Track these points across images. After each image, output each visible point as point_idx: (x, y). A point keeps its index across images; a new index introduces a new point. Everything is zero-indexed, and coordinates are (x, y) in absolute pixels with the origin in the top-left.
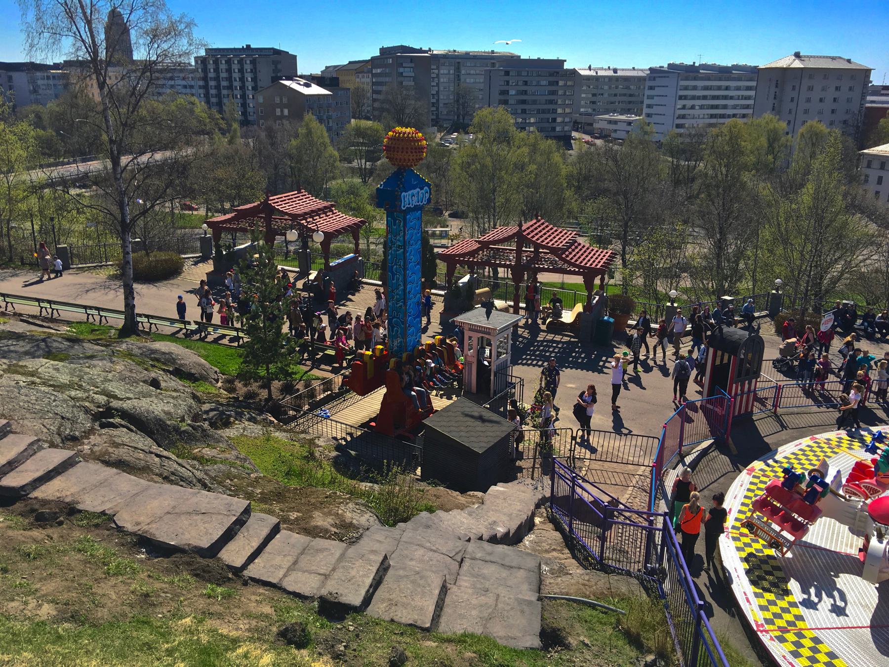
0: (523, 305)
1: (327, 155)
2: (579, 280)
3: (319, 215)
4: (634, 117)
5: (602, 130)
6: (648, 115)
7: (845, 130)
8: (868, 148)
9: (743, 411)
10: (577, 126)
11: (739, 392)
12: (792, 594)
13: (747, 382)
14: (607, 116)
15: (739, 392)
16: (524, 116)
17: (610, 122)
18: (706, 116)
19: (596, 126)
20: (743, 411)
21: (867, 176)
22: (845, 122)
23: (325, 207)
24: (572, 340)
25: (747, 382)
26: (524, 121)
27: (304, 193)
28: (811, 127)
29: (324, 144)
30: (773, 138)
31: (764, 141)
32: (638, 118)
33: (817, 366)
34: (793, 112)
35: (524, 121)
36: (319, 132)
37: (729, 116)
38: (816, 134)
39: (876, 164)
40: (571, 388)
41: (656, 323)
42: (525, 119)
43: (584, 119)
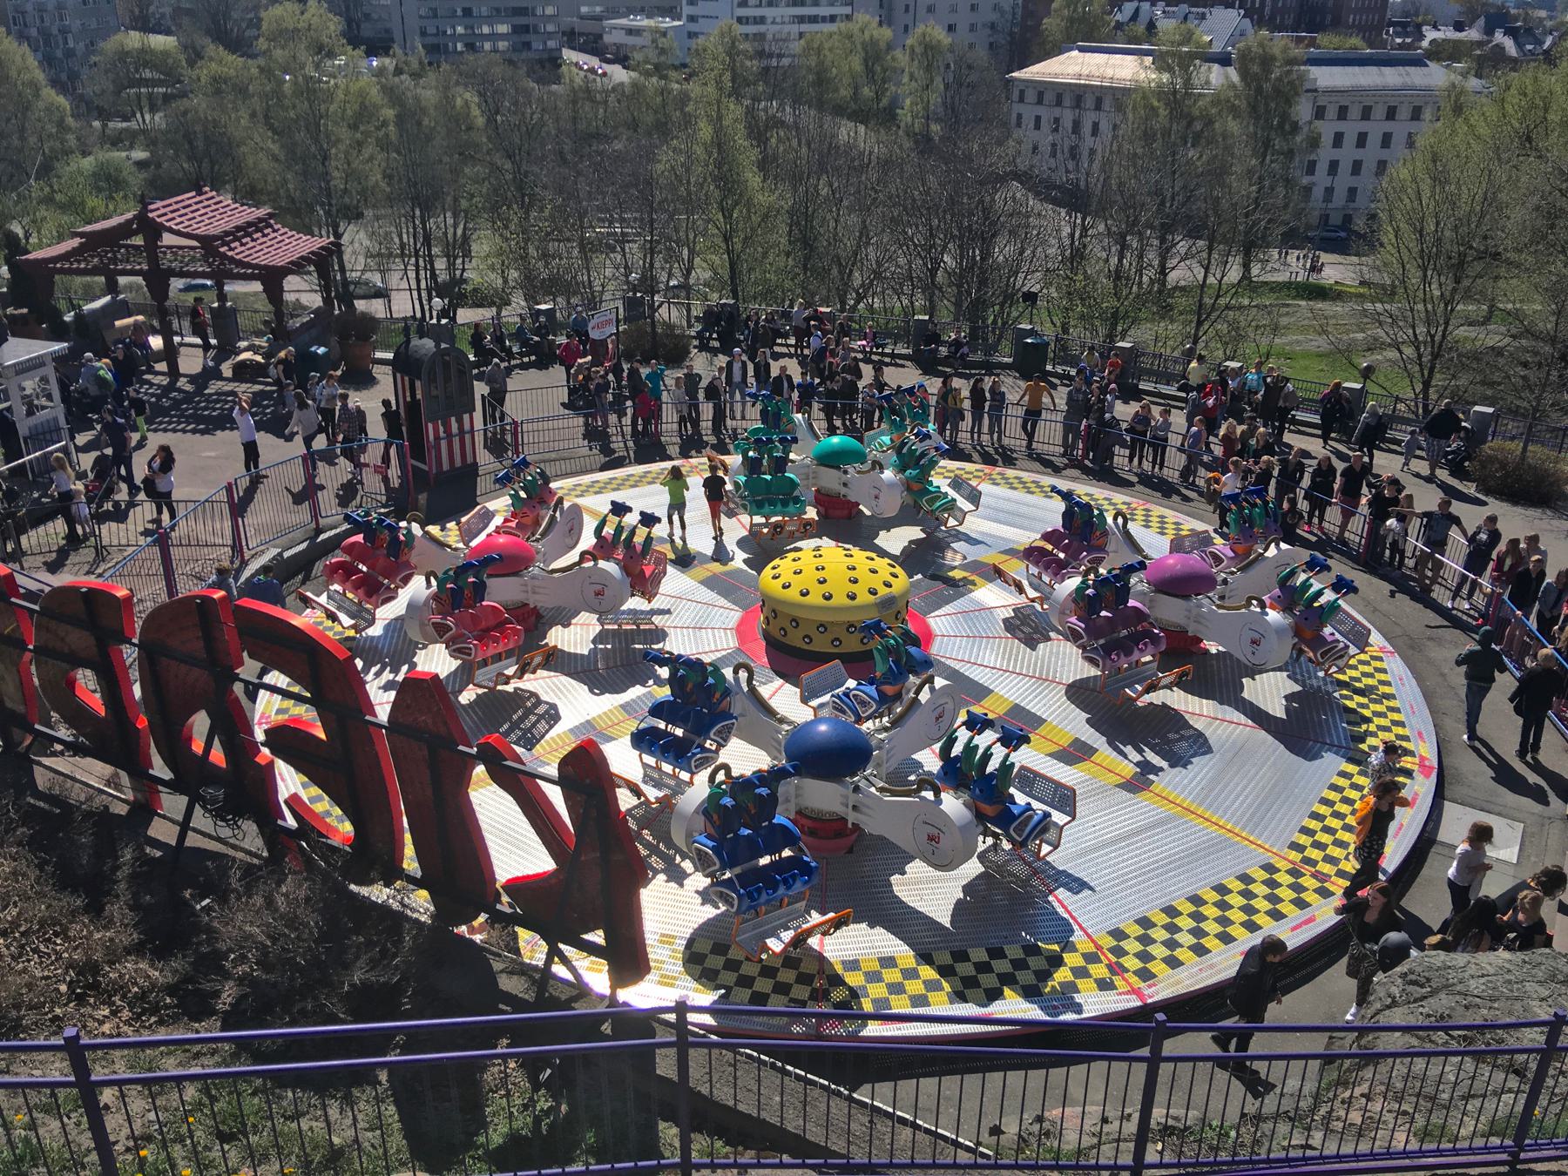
0: (213, 342)
1: (41, 104)
2: (257, 286)
3: (238, 239)
4: (668, 23)
5: (618, 46)
6: (692, 19)
7: (991, 40)
8: (1021, 67)
9: (458, 463)
10: (572, 38)
11: (442, 434)
12: (1040, 721)
13: (453, 419)
14: (623, 21)
15: (442, 434)
16: (468, 21)
17: (630, 31)
18: (787, 20)
19: (607, 39)
20: (458, 463)
21: (1020, 116)
22: (993, 26)
23: (260, 220)
24: (269, 388)
25: (453, 419)
26: (469, 31)
27: (210, 195)
28: (924, 35)
29: (35, 87)
30: (874, 56)
31: (856, 63)
32: (677, 23)
33: (339, 373)
34: (912, 8)
35: (469, 31)
36: (18, 59)
37: (824, 19)
38: (932, 48)
39: (1031, 96)
40: (210, 457)
41: (386, 348)
42: (472, 28)
43: (590, 26)
